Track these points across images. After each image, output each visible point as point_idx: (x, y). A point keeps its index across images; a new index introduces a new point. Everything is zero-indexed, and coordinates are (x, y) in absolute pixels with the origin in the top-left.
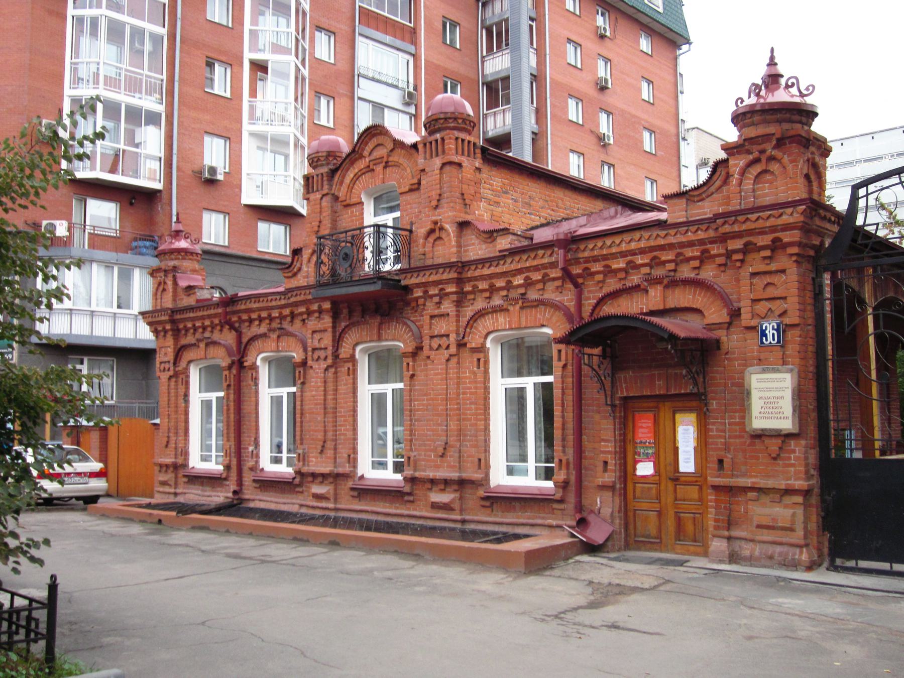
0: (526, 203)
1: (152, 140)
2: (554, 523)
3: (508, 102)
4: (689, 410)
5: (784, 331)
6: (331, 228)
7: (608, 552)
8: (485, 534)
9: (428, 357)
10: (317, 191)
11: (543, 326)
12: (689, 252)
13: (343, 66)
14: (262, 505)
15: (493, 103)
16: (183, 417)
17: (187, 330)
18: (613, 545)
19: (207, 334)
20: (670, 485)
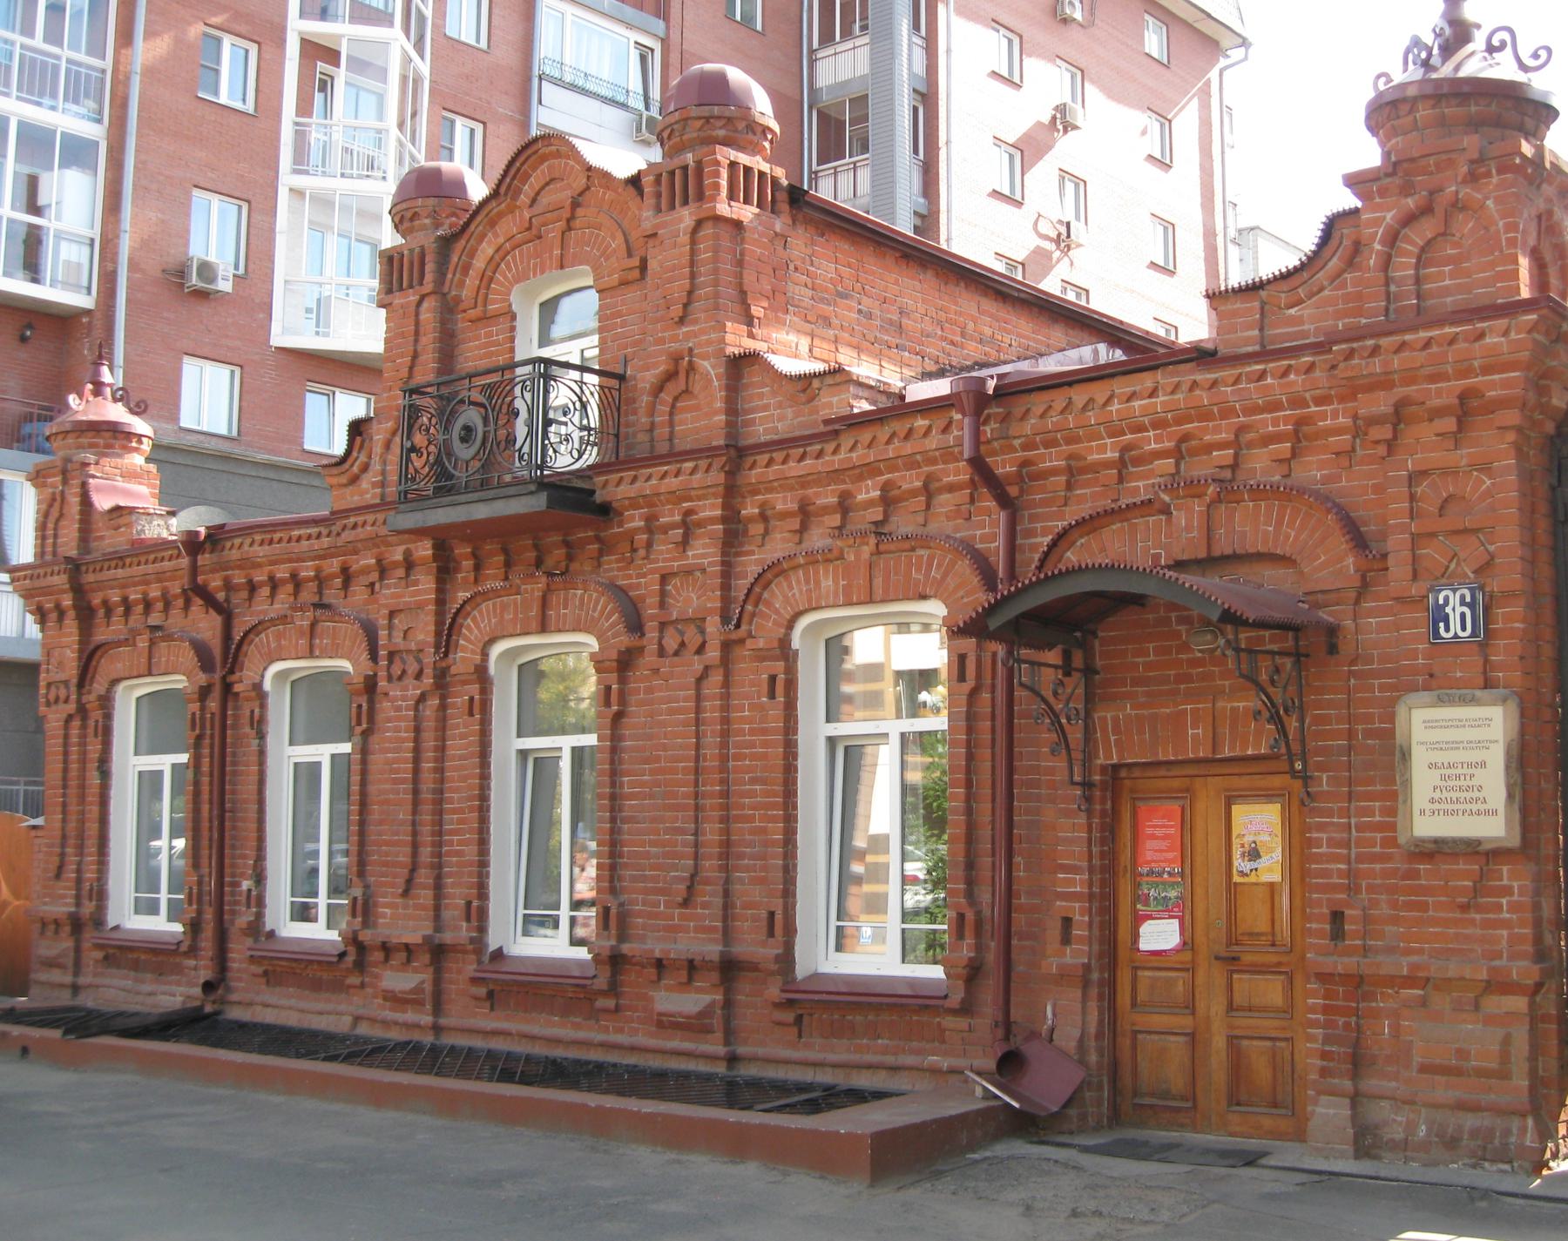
0: (891, 322)
1: (73, 200)
2: (945, 1063)
3: (865, 148)
4: (1267, 796)
5: (1487, 609)
6: (440, 372)
7: (1071, 1133)
8: (782, 1088)
9: (656, 671)
10: (411, 286)
11: (923, 597)
12: (1267, 423)
13: (506, 55)
14: (268, 1017)
15: (831, 149)
16: (95, 809)
17: (109, 609)
18: (1083, 1117)
19: (155, 619)
20: (1218, 976)
